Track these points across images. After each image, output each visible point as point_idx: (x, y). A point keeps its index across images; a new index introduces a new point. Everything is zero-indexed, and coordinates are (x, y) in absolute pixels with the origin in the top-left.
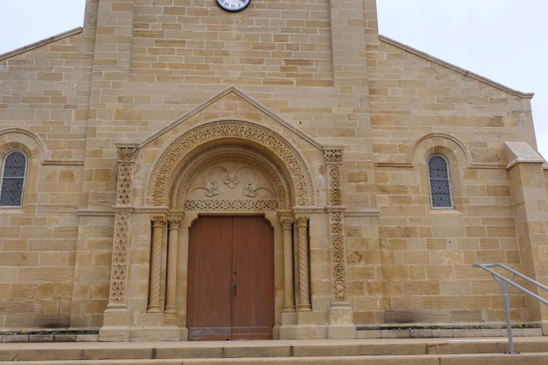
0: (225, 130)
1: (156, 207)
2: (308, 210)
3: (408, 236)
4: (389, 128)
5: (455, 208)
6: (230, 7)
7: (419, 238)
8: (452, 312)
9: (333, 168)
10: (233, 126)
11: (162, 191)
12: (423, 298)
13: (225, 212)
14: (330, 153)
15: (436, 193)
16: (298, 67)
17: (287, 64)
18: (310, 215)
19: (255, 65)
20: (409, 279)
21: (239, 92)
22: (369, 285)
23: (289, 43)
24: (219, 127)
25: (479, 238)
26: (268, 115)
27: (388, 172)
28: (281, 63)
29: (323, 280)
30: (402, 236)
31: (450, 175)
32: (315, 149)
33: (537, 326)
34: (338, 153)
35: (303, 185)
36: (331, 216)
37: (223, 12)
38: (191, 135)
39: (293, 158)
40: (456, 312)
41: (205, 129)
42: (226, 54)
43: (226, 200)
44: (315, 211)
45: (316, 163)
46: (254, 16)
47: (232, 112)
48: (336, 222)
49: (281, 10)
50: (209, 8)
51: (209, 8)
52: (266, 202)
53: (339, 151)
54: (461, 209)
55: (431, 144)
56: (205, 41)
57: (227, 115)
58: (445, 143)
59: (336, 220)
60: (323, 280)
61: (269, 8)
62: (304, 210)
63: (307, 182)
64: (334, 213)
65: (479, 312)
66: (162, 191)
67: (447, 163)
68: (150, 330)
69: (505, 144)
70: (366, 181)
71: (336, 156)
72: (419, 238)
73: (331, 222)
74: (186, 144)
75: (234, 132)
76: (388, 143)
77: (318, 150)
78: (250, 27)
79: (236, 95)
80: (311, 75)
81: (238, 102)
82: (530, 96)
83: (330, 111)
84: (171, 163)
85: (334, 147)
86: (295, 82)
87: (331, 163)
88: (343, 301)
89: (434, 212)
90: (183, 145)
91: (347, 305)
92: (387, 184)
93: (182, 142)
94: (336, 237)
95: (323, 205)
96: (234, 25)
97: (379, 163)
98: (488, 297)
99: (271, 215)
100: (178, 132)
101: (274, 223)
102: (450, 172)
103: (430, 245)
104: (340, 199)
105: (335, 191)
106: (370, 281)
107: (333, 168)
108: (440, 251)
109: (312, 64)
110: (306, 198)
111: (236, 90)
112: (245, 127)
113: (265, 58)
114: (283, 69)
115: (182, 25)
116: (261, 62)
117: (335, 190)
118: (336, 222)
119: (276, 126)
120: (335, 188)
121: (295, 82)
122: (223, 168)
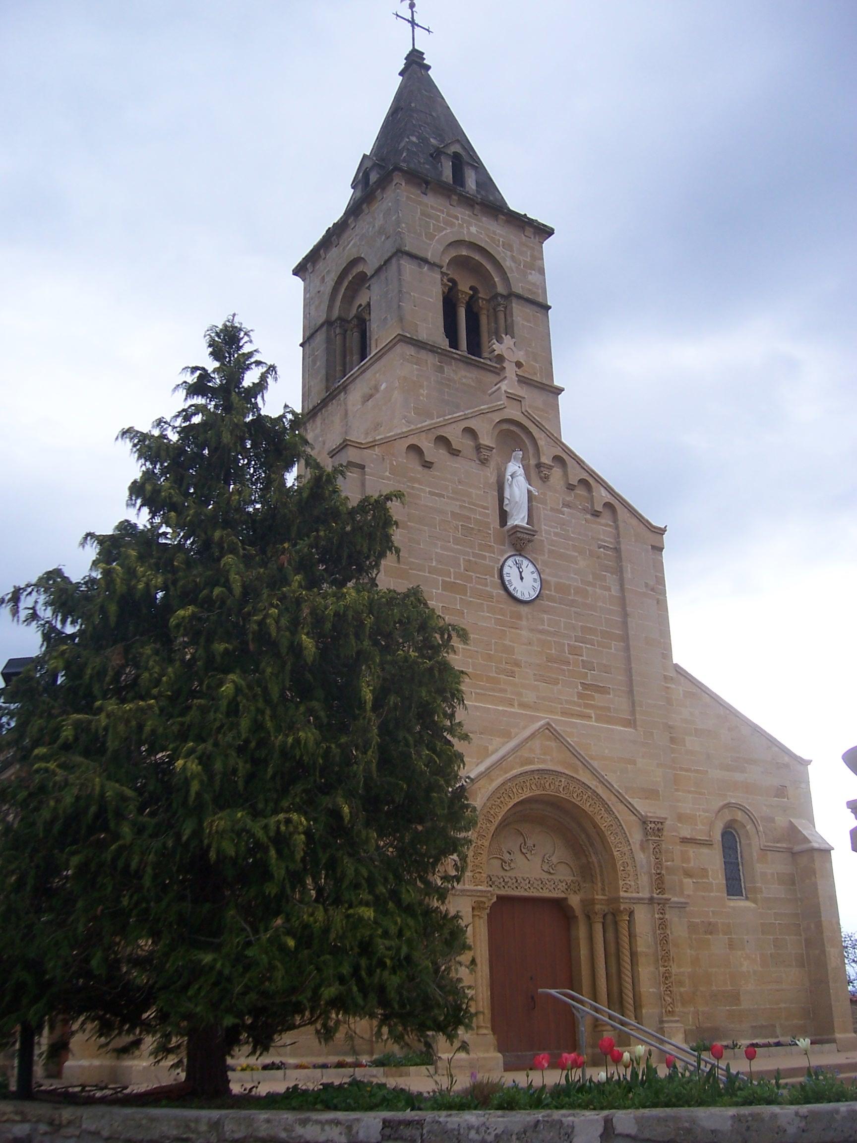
0: (542, 782)
1: (475, 888)
2: (634, 898)
3: (711, 933)
4: (689, 792)
5: (747, 898)
6: (519, 595)
7: (721, 936)
8: (752, 1027)
9: (655, 845)
10: (581, 790)
11: (481, 865)
12: (728, 1010)
13: (526, 894)
14: (653, 825)
15: (729, 879)
16: (596, 695)
17: (584, 689)
18: (634, 906)
19: (550, 686)
20: (714, 988)
21: (555, 730)
22: (681, 994)
23: (585, 658)
24: (536, 777)
25: (771, 937)
26: (587, 766)
27: (691, 851)
28: (577, 687)
29: (651, 990)
30: (706, 933)
31: (741, 857)
32: (634, 817)
33: (833, 1041)
34: (659, 826)
35: (626, 865)
36: (657, 908)
37: (510, 601)
38: (507, 787)
39: (614, 827)
40: (755, 1027)
41: (521, 779)
42: (517, 664)
43: (526, 876)
44: (640, 901)
45: (636, 836)
46: (545, 612)
47: (548, 757)
48: (661, 916)
49: (573, 609)
50: (495, 592)
51: (495, 592)
52: (569, 882)
53: (661, 823)
54: (755, 901)
55: (727, 816)
56: (493, 641)
57: (544, 761)
58: (740, 816)
59: (662, 913)
60: (651, 990)
61: (560, 603)
62: (630, 899)
63: (629, 861)
64: (659, 904)
65: (774, 1026)
66: (481, 865)
67: (738, 840)
68: (485, 1058)
69: (790, 821)
70: (673, 861)
71: (658, 830)
72: (721, 936)
73: (657, 916)
74: (502, 799)
75: (552, 787)
76: (688, 812)
77: (637, 819)
78: (541, 627)
79: (551, 734)
80: (609, 709)
81: (553, 744)
82: (809, 762)
83: (634, 763)
84: (488, 825)
85: (657, 818)
86: (593, 715)
87: (653, 838)
88: (672, 1016)
89: (732, 904)
90: (499, 801)
91: (677, 1021)
92: (690, 865)
93: (498, 795)
94: (662, 936)
95: (647, 895)
96: (524, 623)
97: (683, 838)
98: (780, 1008)
99: (574, 901)
100: (492, 780)
101: (578, 911)
102: (741, 852)
103: (731, 945)
104: (663, 886)
105: (658, 876)
106: (682, 990)
107: (655, 845)
108: (739, 953)
109: (609, 694)
110: (629, 883)
111: (553, 727)
112: (563, 780)
113: (560, 677)
114: (580, 696)
115: (466, 611)
116: (556, 682)
117: (659, 874)
118: (661, 916)
119: (594, 783)
120: (658, 871)
121: (593, 715)
122: (519, 831)
